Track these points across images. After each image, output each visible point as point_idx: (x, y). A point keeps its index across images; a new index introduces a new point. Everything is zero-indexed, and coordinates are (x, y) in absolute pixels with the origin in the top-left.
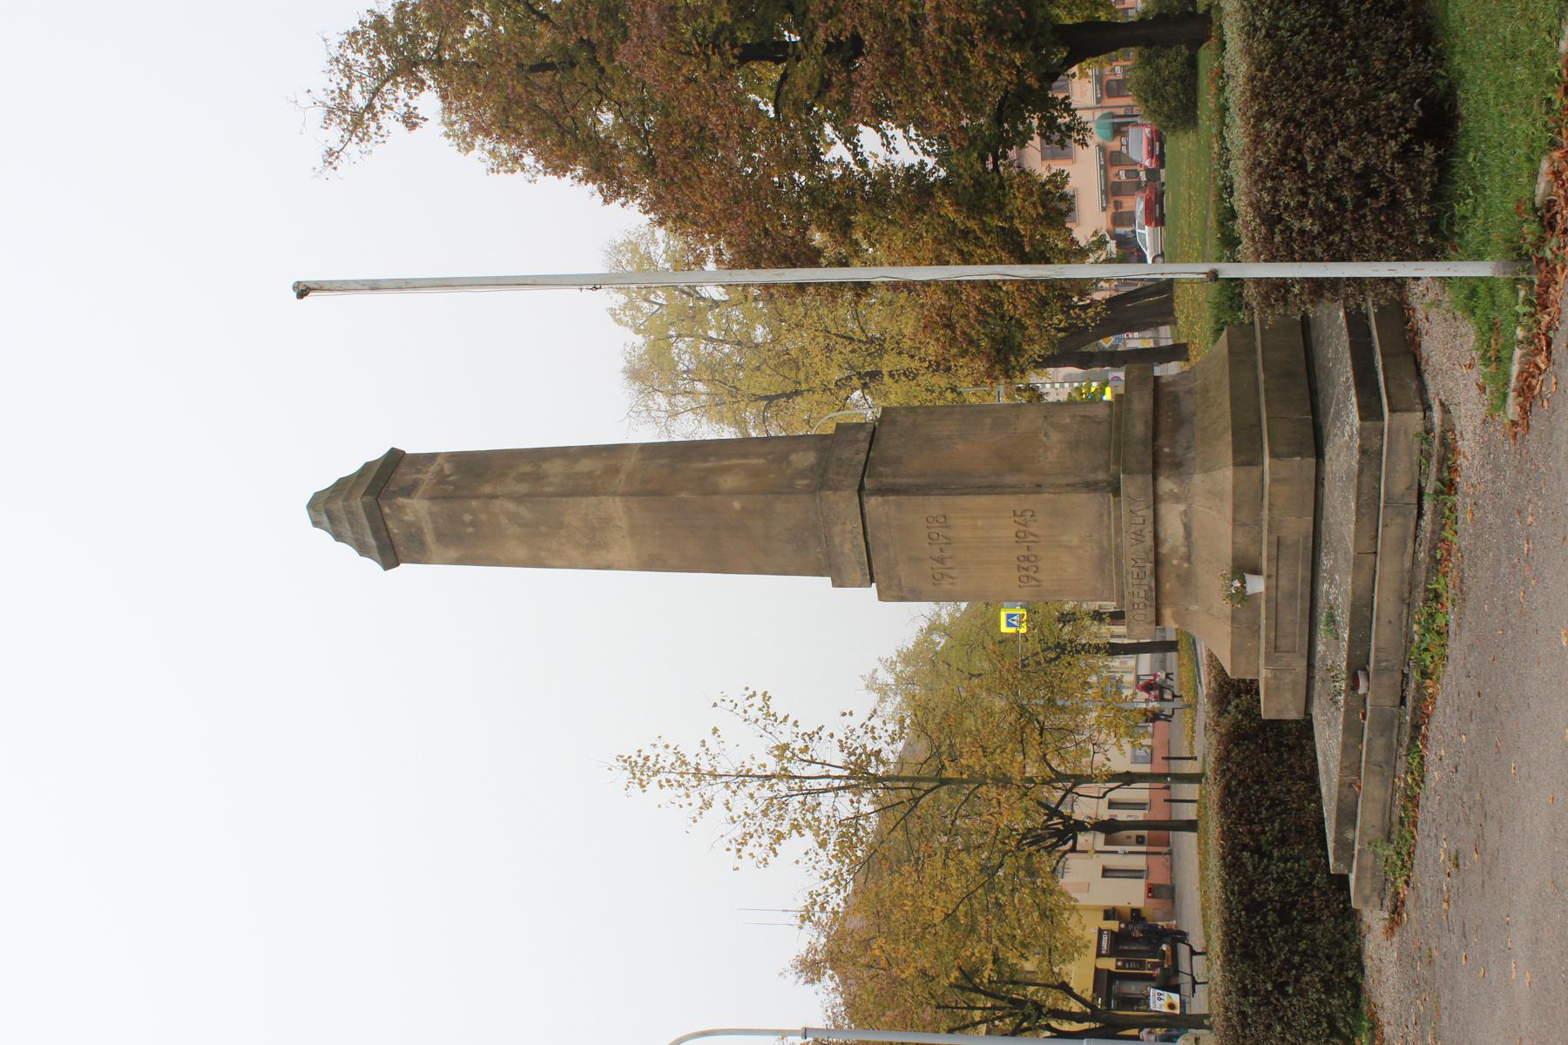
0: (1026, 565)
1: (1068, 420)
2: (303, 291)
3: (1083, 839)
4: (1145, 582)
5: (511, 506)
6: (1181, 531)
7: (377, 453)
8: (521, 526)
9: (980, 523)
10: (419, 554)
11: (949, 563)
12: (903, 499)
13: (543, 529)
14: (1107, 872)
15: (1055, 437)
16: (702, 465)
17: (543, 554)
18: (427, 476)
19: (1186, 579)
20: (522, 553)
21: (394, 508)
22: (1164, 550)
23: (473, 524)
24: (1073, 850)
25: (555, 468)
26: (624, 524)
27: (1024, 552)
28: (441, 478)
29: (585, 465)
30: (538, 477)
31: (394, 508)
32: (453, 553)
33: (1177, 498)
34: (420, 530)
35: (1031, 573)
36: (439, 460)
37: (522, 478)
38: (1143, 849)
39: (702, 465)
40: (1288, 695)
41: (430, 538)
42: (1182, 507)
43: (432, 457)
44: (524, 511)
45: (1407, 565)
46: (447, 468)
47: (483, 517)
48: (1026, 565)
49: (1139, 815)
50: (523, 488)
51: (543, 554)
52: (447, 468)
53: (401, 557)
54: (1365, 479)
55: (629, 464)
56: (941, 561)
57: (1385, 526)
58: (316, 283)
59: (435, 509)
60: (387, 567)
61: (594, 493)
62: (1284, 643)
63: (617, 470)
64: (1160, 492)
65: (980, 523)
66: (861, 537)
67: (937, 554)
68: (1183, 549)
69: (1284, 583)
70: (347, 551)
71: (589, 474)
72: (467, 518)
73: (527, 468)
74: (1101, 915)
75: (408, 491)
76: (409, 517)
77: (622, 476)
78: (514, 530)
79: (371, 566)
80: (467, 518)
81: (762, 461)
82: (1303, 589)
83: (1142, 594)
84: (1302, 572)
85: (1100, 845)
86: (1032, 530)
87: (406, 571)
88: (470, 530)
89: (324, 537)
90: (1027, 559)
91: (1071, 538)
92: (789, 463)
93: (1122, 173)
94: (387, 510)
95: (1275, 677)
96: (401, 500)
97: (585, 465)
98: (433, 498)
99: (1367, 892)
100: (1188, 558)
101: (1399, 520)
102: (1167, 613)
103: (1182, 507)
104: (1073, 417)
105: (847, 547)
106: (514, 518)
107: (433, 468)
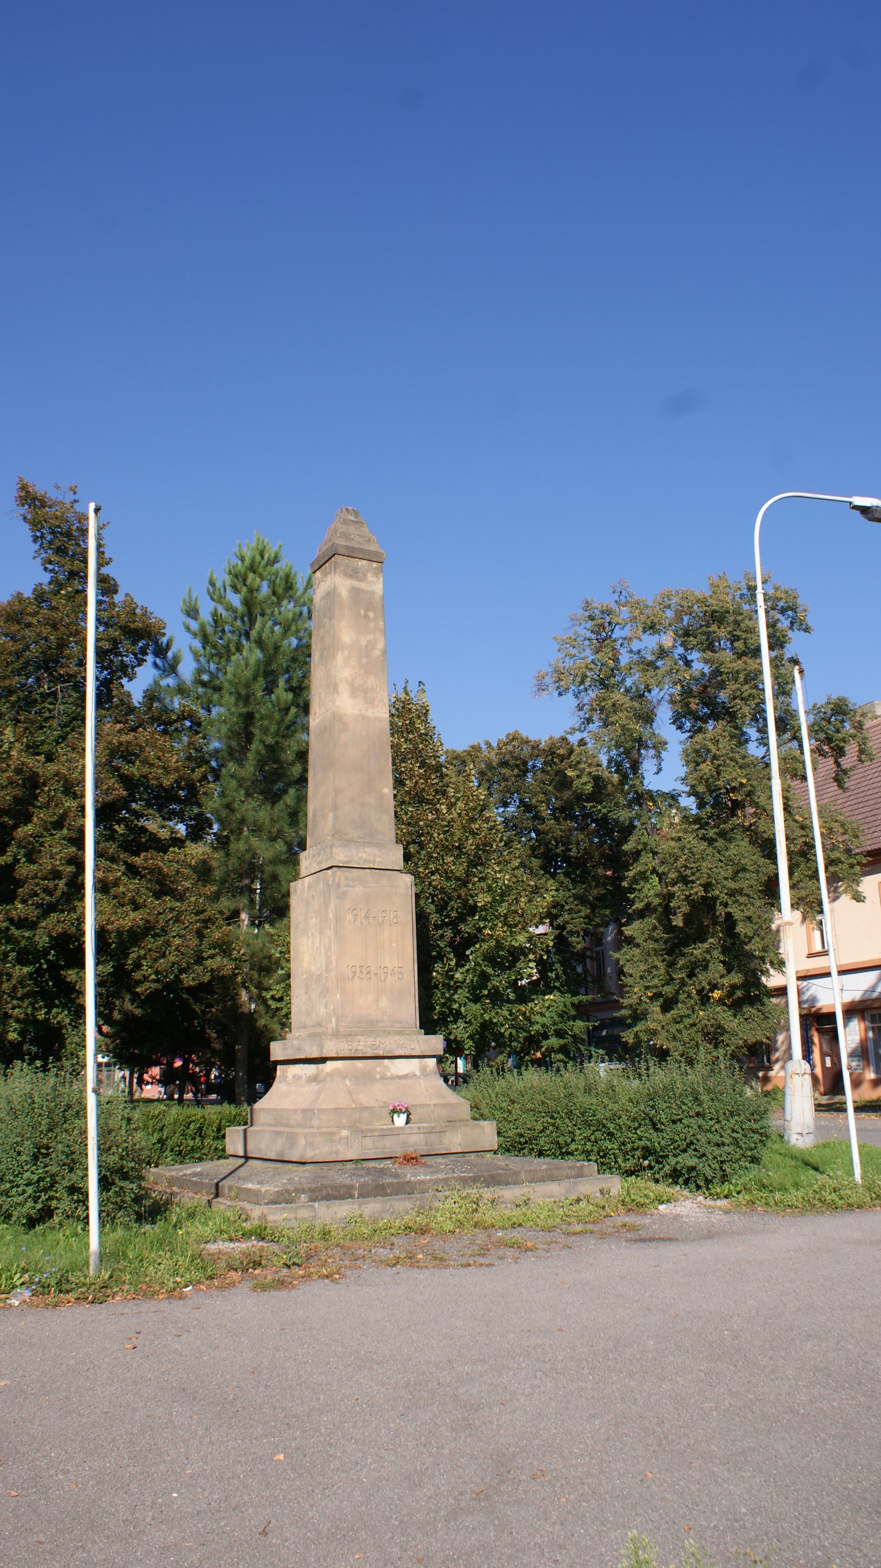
4: (369, 1050)
8: (367, 646)
9: (394, 945)
23: (366, 616)
34: (361, 580)
41: (356, 583)
76: (370, 576)
80: (371, 615)
86: (389, 977)
105: (364, 856)
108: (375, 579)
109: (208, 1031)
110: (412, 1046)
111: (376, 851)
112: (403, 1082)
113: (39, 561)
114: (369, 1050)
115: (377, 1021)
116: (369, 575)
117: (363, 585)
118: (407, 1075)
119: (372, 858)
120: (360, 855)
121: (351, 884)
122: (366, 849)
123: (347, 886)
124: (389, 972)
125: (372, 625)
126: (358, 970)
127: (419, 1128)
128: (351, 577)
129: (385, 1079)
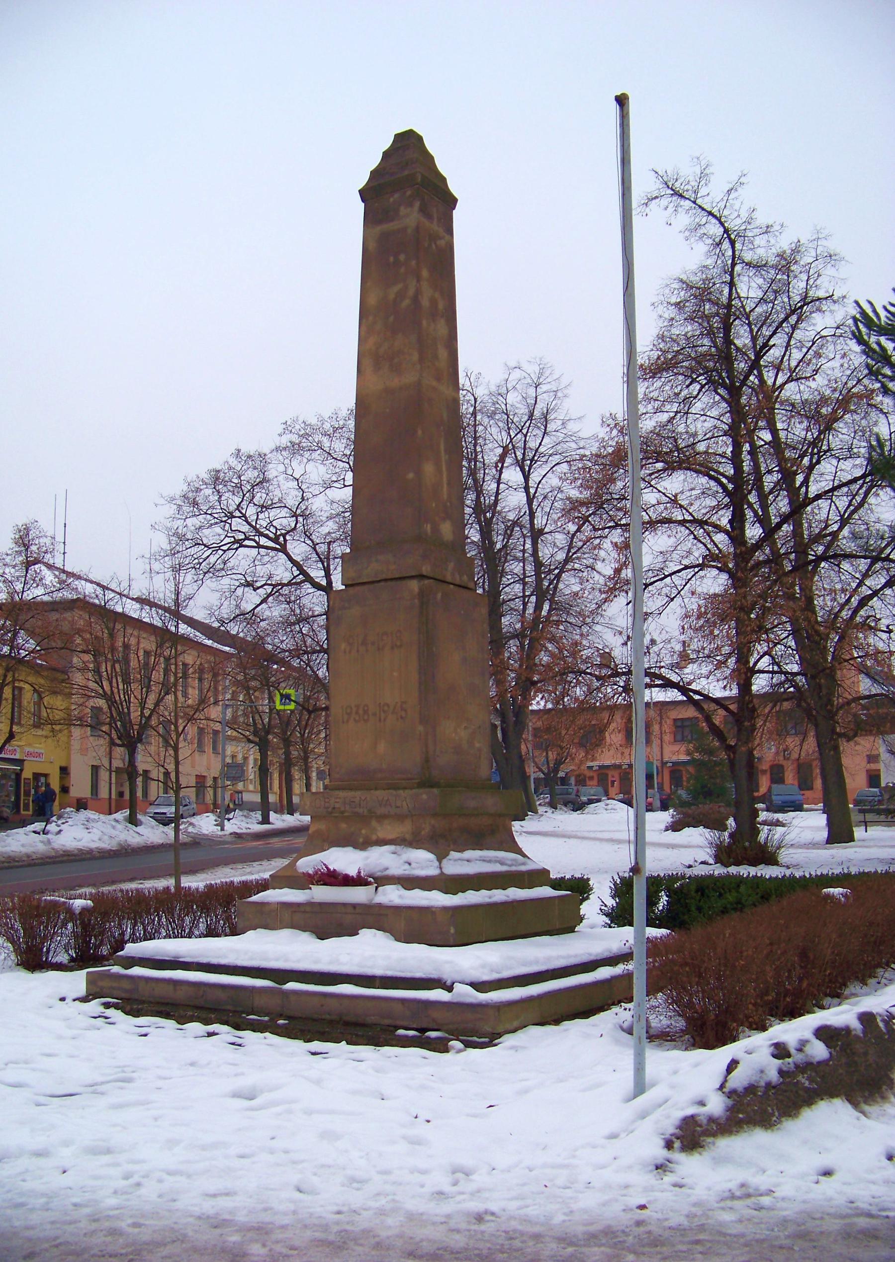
0: (361, 712)
1: (477, 745)
2: (622, 101)
3: (120, 752)
4: (348, 807)
5: (411, 292)
7: (454, 187)
13: (391, 319)
14: (95, 769)
15: (463, 734)
16: (442, 447)
18: (435, 227)
20: (372, 300)
21: (408, 200)
24: (112, 743)
25: (442, 328)
28: (434, 238)
29: (443, 353)
30: (434, 315)
31: (408, 200)
32: (372, 246)
36: (447, 237)
37: (433, 302)
38: (113, 796)
39: (442, 447)
43: (450, 231)
44: (406, 302)
46: (442, 243)
47: (402, 270)
48: (361, 712)
49: (139, 794)
50: (425, 303)
51: (371, 318)
52: (442, 243)
55: (445, 390)
56: (364, 643)
58: (628, 113)
59: (409, 231)
61: (421, 360)
63: (438, 379)
65: (395, 674)
70: (375, 160)
71: (436, 357)
72: (402, 257)
73: (441, 305)
74: (64, 764)
75: (423, 210)
76: (403, 211)
77: (434, 383)
81: (445, 497)
85: (117, 763)
87: (355, 211)
89: (387, 143)
90: (366, 712)
91: (382, 747)
92: (444, 519)
96: (417, 204)
97: (443, 353)
98: (417, 229)
104: (480, 750)
106: (401, 295)
107: (441, 231)
108: (409, 209)
110: (399, 804)
126: (354, 710)
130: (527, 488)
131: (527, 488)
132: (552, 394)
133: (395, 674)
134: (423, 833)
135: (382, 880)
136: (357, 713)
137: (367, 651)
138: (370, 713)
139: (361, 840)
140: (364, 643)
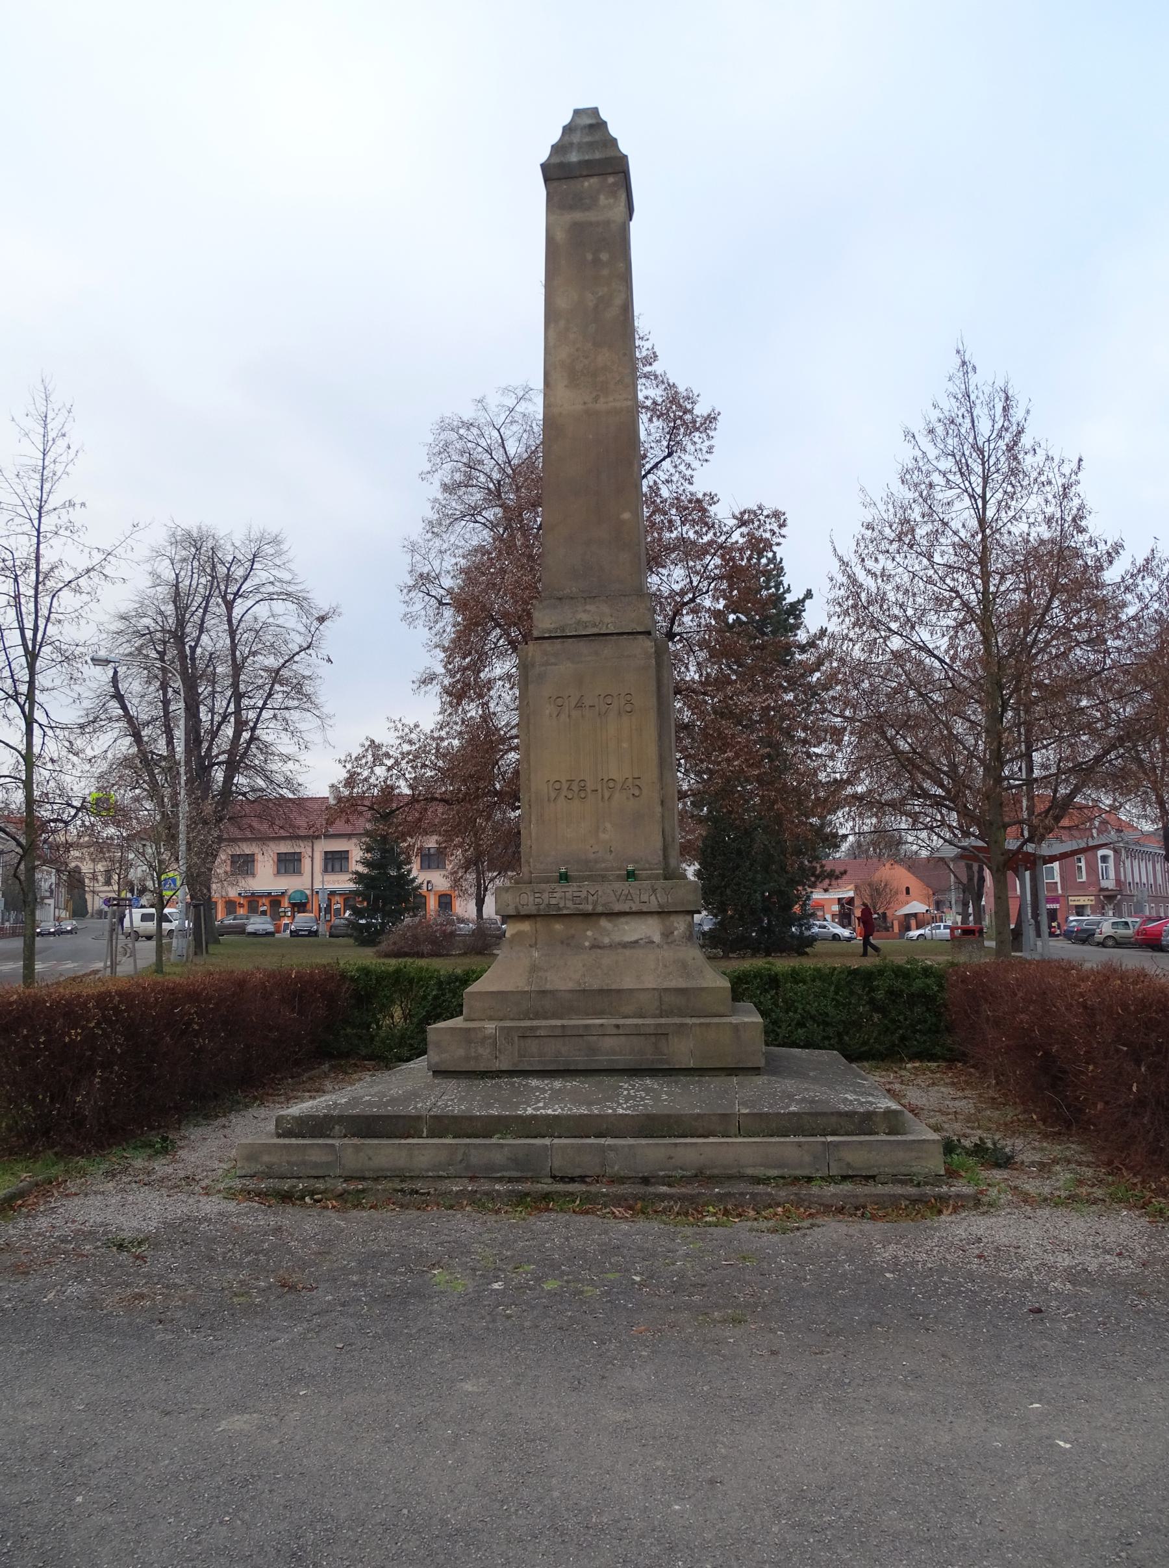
0: (575, 788)
4: (569, 904)
6: (628, 938)
8: (596, 306)
9: (625, 745)
10: (554, 203)
11: (574, 713)
12: (652, 672)
17: (562, 323)
19: (569, 943)
20: (562, 303)
22: (604, 923)
23: (596, 261)
26: (601, 406)
27: (590, 786)
32: (560, 236)
33: (667, 935)
34: (588, 209)
35: (564, 792)
40: (461, 1052)
41: (578, 216)
42: (657, 938)
45: (750, 1171)
48: (575, 788)
51: (562, 323)
53: (555, 184)
54: (834, 1119)
56: (579, 706)
57: (799, 1145)
60: (545, 167)
62: (533, 1046)
64: (673, 918)
66: (595, 630)
67: (588, 702)
68: (606, 941)
69: (608, 1043)
70: (555, 136)
76: (603, 200)
78: (590, 300)
79: (544, 155)
80: (604, 257)
82: (602, 1061)
83: (553, 901)
84: (624, 1059)
86: (617, 795)
88: (589, 257)
89: (567, 119)
90: (583, 789)
93: (338, 906)
94: (611, 180)
95: (485, 1038)
99: (266, 1158)
100: (595, 946)
101: (807, 1158)
102: (525, 927)
103: (657, 938)
105: (584, 617)
108: (612, 201)
109: (1147, 827)
110: (645, 898)
111: (605, 609)
112: (628, 952)
113: (907, 454)
114: (569, 904)
115: (596, 862)
116: (602, 197)
117: (591, 216)
118: (636, 942)
119: (597, 620)
120: (578, 616)
121: (553, 661)
122: (588, 607)
123: (547, 664)
124: (619, 786)
125: (605, 272)
126: (565, 786)
127: (617, 1026)
128: (572, 208)
129: (599, 947)
130: (230, 621)
131: (230, 621)
132: (253, 633)
133: (625, 745)
134: (676, 933)
135: (722, 1125)
136: (569, 789)
137: (583, 716)
138: (589, 790)
139: (587, 944)
140: (579, 706)
